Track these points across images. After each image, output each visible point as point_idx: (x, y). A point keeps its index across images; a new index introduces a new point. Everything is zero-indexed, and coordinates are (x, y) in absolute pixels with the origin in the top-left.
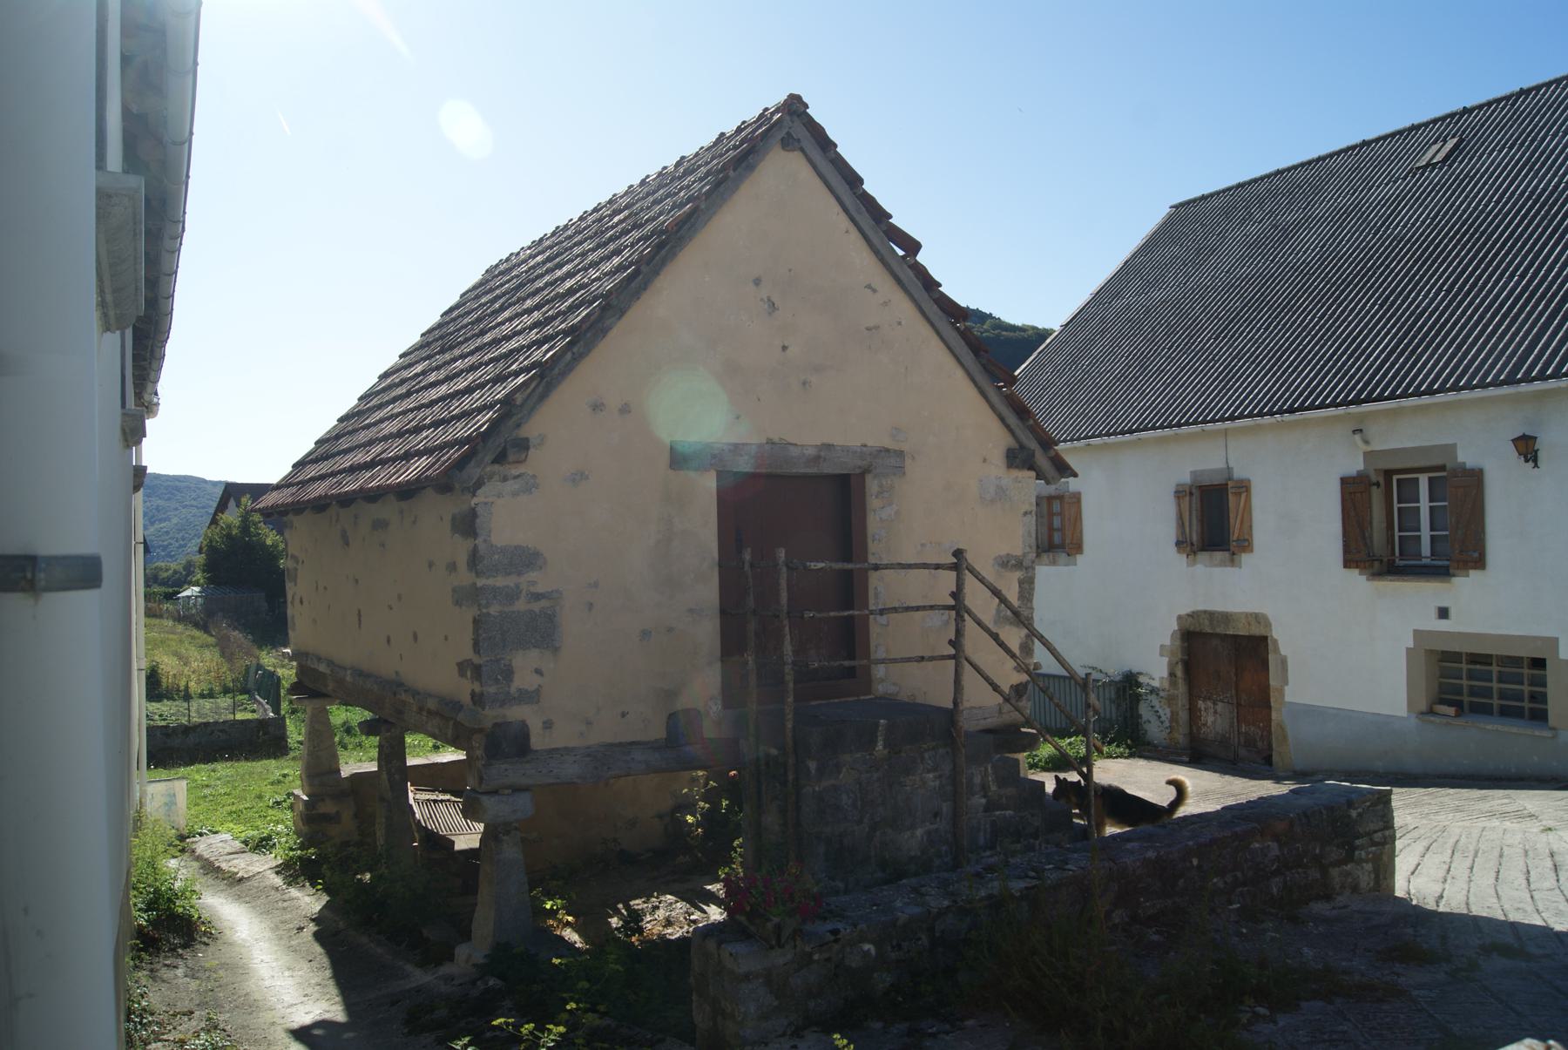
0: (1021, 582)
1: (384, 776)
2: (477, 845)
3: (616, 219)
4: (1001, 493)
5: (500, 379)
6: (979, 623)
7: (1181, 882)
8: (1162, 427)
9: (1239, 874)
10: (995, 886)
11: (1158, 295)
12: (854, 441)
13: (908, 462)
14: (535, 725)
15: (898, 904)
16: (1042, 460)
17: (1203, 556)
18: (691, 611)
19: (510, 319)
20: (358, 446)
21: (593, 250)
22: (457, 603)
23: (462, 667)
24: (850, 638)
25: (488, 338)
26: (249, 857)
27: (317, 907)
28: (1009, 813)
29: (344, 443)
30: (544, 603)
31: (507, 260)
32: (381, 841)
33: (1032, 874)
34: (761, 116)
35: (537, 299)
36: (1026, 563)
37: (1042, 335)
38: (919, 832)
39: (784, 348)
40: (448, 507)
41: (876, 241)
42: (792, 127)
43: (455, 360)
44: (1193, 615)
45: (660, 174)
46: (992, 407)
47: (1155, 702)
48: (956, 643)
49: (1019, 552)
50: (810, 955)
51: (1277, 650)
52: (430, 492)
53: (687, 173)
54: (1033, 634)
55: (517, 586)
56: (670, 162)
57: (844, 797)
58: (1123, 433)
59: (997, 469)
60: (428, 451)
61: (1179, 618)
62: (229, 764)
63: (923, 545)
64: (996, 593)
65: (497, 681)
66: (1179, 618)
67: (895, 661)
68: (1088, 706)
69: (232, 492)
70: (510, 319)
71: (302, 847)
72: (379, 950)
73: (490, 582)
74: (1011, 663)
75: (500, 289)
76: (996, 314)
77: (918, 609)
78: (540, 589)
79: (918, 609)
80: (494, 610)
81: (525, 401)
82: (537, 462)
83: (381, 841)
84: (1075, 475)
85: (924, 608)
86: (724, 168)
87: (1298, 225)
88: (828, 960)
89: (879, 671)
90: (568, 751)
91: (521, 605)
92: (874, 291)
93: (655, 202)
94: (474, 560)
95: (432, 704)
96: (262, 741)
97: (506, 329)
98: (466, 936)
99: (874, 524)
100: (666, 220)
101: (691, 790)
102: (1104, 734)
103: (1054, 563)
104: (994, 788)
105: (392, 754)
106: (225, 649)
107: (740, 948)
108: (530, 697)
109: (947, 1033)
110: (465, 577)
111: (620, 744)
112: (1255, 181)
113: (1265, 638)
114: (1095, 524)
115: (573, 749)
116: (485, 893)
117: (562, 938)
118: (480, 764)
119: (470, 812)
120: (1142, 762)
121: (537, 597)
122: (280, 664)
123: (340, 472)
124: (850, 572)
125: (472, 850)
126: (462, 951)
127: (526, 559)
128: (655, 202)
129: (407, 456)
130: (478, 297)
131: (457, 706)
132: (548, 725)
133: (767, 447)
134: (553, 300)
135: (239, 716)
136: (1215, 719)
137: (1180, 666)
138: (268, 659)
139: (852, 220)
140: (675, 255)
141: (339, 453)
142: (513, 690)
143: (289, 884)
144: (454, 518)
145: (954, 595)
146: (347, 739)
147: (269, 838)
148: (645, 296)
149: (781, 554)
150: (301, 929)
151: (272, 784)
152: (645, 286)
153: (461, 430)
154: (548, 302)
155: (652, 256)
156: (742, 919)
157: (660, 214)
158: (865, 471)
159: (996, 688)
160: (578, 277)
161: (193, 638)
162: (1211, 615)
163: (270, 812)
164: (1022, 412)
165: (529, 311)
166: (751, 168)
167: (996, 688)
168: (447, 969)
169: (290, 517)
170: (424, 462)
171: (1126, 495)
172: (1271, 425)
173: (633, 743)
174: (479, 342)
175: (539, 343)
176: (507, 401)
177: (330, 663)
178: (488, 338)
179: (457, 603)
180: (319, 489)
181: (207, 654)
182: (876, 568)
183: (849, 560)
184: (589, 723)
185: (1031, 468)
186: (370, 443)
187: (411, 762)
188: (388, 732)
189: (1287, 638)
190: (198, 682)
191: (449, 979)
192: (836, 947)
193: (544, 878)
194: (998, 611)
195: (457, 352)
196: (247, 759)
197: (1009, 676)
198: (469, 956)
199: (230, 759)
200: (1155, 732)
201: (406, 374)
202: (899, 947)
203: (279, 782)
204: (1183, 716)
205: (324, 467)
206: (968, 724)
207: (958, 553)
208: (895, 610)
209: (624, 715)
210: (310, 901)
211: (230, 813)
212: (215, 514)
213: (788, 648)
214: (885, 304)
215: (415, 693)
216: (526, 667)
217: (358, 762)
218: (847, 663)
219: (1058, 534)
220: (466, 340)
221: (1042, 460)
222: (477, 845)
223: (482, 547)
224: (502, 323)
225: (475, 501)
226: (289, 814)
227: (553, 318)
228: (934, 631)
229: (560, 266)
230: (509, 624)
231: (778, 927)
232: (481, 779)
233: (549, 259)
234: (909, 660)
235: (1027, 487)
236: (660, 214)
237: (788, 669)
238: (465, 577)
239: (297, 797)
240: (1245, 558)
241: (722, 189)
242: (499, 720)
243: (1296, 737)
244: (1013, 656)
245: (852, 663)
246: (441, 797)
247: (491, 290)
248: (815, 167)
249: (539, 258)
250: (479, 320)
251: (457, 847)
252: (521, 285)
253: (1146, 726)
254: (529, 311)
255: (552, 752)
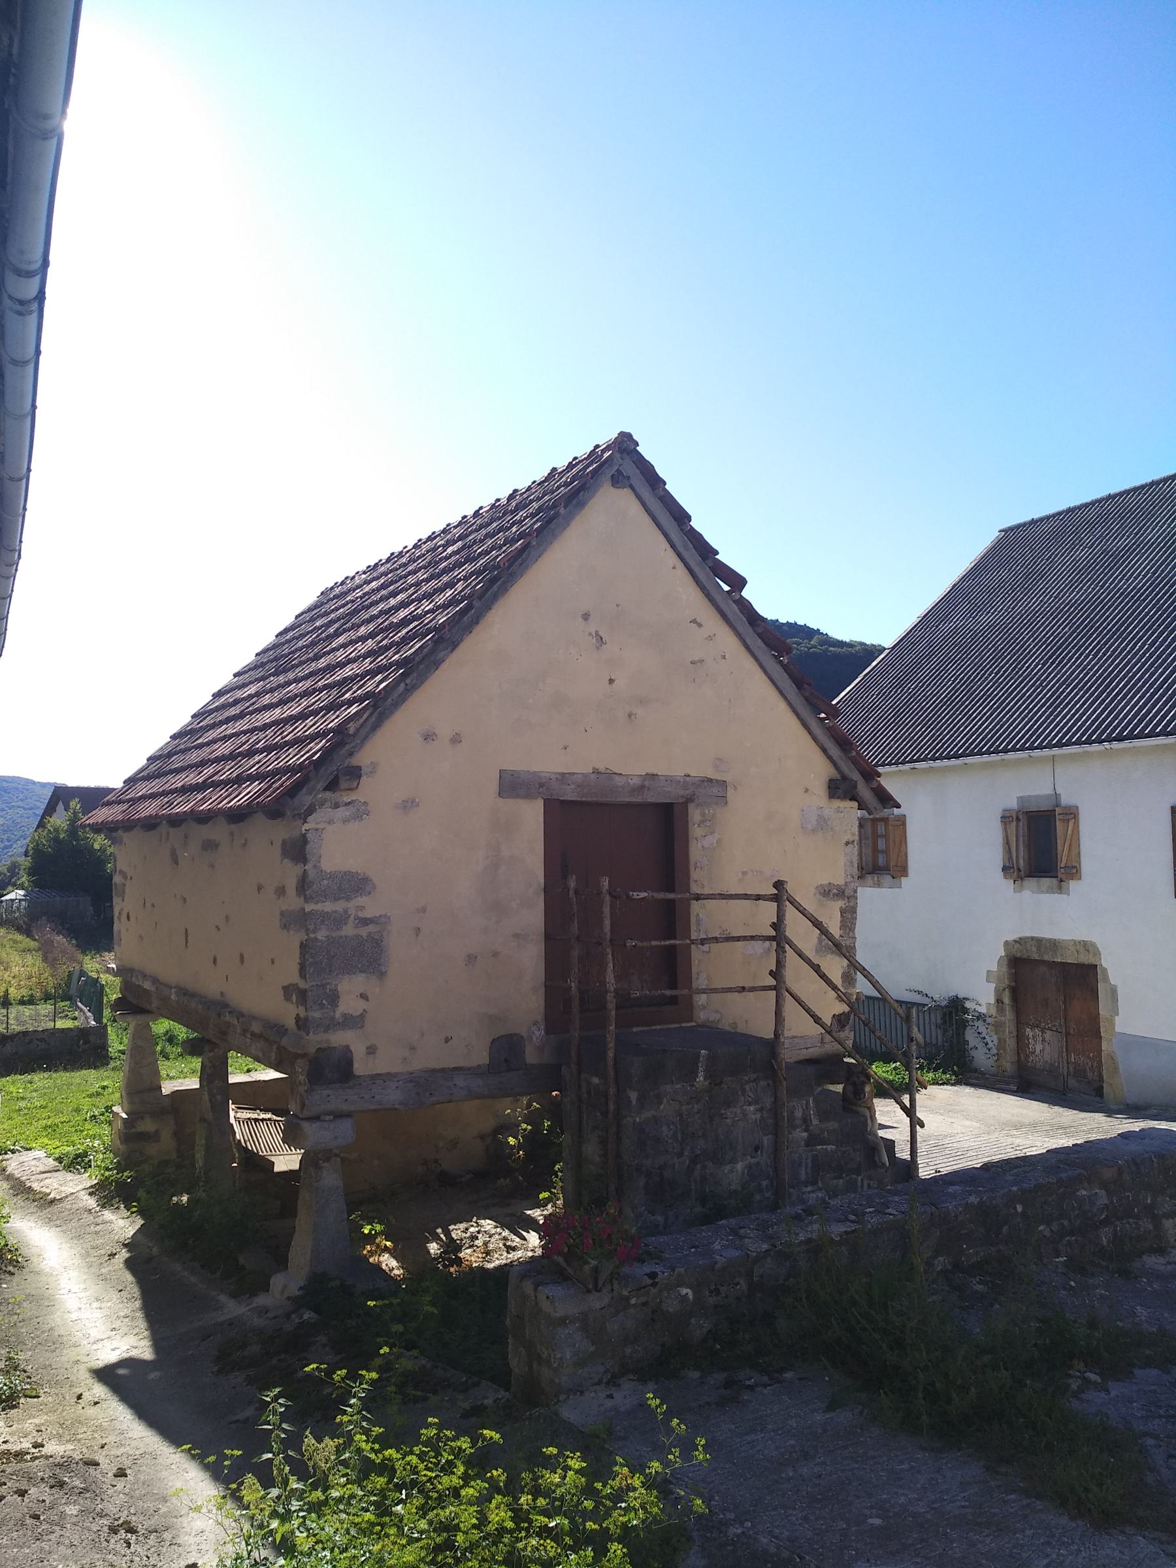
0: (843, 912)
1: (206, 1097)
2: (296, 1166)
3: (450, 550)
4: (823, 824)
5: (332, 707)
6: (800, 955)
7: (1005, 1229)
8: (988, 752)
9: (1066, 1223)
10: (813, 1230)
11: (985, 619)
12: (678, 772)
13: (730, 791)
14: (358, 1050)
15: (717, 1246)
16: (863, 790)
17: (1031, 882)
18: (517, 936)
19: (344, 646)
20: (190, 766)
21: (427, 580)
22: (285, 927)
23: (288, 990)
24: (673, 967)
25: (322, 663)
26: (64, 1176)
27: (131, 1232)
28: (829, 1147)
29: (177, 762)
30: (372, 928)
31: (343, 583)
32: (200, 1163)
33: (852, 1217)
34: (592, 452)
35: (371, 627)
36: (848, 892)
37: (871, 652)
38: (740, 1166)
39: (611, 681)
40: (280, 831)
41: (702, 576)
42: (620, 465)
43: (289, 683)
44: (1020, 941)
45: (493, 506)
46: (815, 739)
47: (982, 1029)
48: (776, 974)
49: (841, 882)
50: (628, 1299)
51: (1106, 979)
52: (260, 818)
53: (518, 508)
54: (855, 966)
55: (346, 911)
56: (504, 494)
57: (665, 1129)
58: (949, 757)
59: (819, 796)
60: (260, 777)
61: (1006, 943)
62: (46, 1075)
63: (744, 873)
64: (817, 924)
65: (322, 1006)
66: (1006, 943)
67: (715, 991)
68: (912, 1040)
69: (61, 795)
70: (344, 646)
71: (120, 1168)
72: (193, 1279)
73: (319, 907)
74: (832, 994)
75: (334, 615)
76: (823, 630)
77: (738, 939)
78: (368, 914)
79: (738, 939)
80: (321, 935)
81: (358, 730)
82: (367, 790)
83: (200, 1163)
84: (899, 806)
85: (745, 938)
86: (554, 506)
87: (1128, 550)
88: (645, 1304)
89: (701, 999)
90: (390, 1076)
91: (349, 930)
92: (700, 625)
93: (489, 536)
94: (303, 885)
95: (256, 1028)
96: (82, 1051)
97: (340, 655)
98: (282, 1262)
99: (696, 852)
100: (498, 556)
101: (514, 1111)
102: (930, 1059)
103: (878, 885)
104: (815, 1122)
105: (214, 1074)
106: (48, 954)
107: (557, 1291)
108: (353, 1022)
109: (765, 1386)
110: (293, 902)
111: (443, 1070)
112: (1086, 505)
113: (1094, 967)
114: (920, 845)
115: (396, 1075)
116: (303, 1222)
117: (378, 1266)
118: (302, 1089)
119: (291, 1137)
120: (968, 1090)
121: (365, 922)
122: (102, 968)
123: (172, 792)
124: (673, 901)
125: (291, 1172)
126: (278, 1281)
127: (356, 884)
128: (489, 536)
129: (239, 780)
130: (312, 620)
131: (281, 1030)
132: (371, 1050)
133: (593, 777)
134: (386, 629)
135: (61, 1024)
136: (1044, 1047)
137: (1007, 993)
138: (92, 965)
139: (679, 555)
140: (506, 590)
141: (171, 772)
142: (338, 1015)
143: (103, 1206)
144: (284, 843)
145: (774, 926)
146: (168, 1048)
147: (85, 1154)
148: (478, 630)
149: (605, 883)
150: (113, 1255)
151: (90, 1096)
152: (476, 621)
153: (293, 757)
154: (382, 631)
155: (485, 590)
156: (560, 1260)
157: (492, 549)
158: (689, 800)
159: (817, 1020)
160: (412, 608)
161: (15, 942)
162: (1039, 941)
163: (87, 1126)
164: (844, 743)
165: (363, 639)
166: (582, 505)
167: (817, 1020)
168: (261, 1300)
169: (120, 832)
170: (255, 787)
171: (953, 815)
172: (1098, 752)
173: (456, 1069)
174: (313, 666)
175: (373, 673)
176: (340, 730)
177: (155, 981)
178: (322, 663)
179: (285, 927)
180: (149, 809)
181: (29, 959)
182: (698, 897)
183: (672, 890)
184: (412, 1048)
185: (853, 799)
186: (203, 764)
187: (232, 1079)
188: (209, 1048)
189: (1118, 968)
190: (19, 987)
191: (263, 1311)
192: (653, 1291)
193: (364, 1202)
194: (820, 941)
195: (291, 675)
196: (65, 1069)
197: (830, 1007)
198: (285, 1285)
199: (48, 1069)
200: (982, 1058)
201: (239, 694)
202: (717, 1291)
203: (98, 1094)
204: (1011, 1043)
205: (155, 786)
206: (789, 1055)
207: (779, 885)
208: (716, 940)
209: (447, 1040)
210: (123, 1225)
211: (46, 1127)
212: (43, 817)
213: (610, 977)
214: (710, 638)
215: (240, 1015)
216: (351, 991)
217: (180, 1078)
218: (668, 992)
219: (881, 855)
220: (301, 663)
221: (863, 790)
222: (296, 1166)
223: (312, 874)
224: (336, 649)
225: (306, 826)
226: (106, 1130)
227: (387, 648)
228: (756, 963)
229: (394, 594)
230: (337, 948)
231: (596, 1270)
232: (303, 1105)
233: (383, 587)
234: (730, 990)
235: (848, 814)
236: (492, 549)
237: (610, 997)
238: (293, 902)
239: (116, 1115)
240: (1073, 884)
241: (552, 526)
242: (324, 1045)
243: (1127, 1071)
244: (835, 988)
245: (674, 993)
246: (263, 1116)
247: (326, 614)
248: (643, 504)
249: (374, 584)
250: (313, 644)
251: (277, 1169)
252: (355, 612)
253: (973, 1053)
254: (363, 639)
255: (375, 1077)
